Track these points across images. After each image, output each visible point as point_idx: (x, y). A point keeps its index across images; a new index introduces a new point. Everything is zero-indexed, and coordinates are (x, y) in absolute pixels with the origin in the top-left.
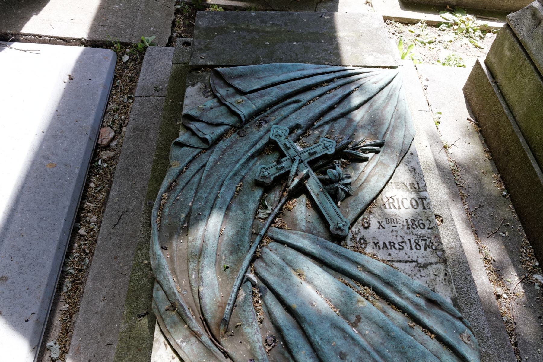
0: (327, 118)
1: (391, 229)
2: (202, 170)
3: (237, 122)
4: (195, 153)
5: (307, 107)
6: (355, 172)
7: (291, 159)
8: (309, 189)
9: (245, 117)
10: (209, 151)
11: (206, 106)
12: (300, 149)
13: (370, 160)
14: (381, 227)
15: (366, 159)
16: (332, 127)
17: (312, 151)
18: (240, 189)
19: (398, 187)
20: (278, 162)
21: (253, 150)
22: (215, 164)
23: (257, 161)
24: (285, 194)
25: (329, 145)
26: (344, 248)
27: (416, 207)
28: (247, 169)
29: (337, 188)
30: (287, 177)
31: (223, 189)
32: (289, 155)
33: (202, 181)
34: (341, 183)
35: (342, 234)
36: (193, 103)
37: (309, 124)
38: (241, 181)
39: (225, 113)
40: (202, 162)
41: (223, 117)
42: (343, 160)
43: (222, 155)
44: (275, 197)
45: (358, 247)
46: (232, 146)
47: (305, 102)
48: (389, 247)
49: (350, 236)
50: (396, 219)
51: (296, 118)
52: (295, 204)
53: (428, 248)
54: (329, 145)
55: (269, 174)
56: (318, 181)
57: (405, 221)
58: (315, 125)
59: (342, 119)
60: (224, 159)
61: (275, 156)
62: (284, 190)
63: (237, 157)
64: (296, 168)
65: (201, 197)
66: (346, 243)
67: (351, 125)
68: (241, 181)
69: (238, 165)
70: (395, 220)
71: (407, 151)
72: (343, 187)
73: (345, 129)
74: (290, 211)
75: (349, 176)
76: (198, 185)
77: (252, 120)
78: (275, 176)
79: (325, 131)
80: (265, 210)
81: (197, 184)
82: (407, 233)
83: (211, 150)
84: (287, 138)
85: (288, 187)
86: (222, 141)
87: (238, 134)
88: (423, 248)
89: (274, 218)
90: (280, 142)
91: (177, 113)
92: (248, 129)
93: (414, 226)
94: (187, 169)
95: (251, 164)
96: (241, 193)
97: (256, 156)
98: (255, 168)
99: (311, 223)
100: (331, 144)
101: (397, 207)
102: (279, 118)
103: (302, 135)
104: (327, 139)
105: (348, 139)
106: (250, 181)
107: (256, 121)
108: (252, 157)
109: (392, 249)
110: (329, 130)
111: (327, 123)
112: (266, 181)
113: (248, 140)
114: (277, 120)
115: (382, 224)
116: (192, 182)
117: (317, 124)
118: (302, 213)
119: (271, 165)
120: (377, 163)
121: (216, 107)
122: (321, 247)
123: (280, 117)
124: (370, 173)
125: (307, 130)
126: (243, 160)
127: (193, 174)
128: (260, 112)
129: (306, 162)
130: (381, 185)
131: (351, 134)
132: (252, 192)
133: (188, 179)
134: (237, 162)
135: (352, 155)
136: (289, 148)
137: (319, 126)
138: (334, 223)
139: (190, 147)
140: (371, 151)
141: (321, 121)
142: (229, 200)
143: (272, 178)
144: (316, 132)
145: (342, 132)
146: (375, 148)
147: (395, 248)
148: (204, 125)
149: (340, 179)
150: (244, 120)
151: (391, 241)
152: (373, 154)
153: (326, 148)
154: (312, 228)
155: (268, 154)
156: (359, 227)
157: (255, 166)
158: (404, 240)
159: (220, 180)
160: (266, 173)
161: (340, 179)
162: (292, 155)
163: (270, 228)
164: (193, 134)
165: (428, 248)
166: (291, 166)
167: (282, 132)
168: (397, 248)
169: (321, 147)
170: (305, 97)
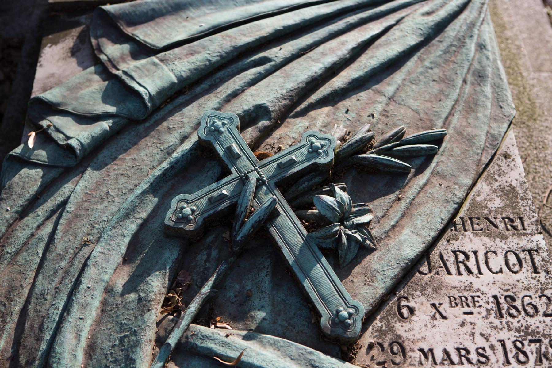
1: (460, 320)
14: (438, 316)
25: (322, 146)
27: (517, 268)
37: (285, 106)
48: (456, 359)
50: (473, 297)
53: (544, 360)
70: (470, 299)
82: (495, 328)
88: (532, 358)
93: (513, 311)
101: (475, 270)
109: (462, 364)
115: (441, 309)
147: (469, 361)
151: (461, 346)
165: (544, 360)
168: (474, 361)
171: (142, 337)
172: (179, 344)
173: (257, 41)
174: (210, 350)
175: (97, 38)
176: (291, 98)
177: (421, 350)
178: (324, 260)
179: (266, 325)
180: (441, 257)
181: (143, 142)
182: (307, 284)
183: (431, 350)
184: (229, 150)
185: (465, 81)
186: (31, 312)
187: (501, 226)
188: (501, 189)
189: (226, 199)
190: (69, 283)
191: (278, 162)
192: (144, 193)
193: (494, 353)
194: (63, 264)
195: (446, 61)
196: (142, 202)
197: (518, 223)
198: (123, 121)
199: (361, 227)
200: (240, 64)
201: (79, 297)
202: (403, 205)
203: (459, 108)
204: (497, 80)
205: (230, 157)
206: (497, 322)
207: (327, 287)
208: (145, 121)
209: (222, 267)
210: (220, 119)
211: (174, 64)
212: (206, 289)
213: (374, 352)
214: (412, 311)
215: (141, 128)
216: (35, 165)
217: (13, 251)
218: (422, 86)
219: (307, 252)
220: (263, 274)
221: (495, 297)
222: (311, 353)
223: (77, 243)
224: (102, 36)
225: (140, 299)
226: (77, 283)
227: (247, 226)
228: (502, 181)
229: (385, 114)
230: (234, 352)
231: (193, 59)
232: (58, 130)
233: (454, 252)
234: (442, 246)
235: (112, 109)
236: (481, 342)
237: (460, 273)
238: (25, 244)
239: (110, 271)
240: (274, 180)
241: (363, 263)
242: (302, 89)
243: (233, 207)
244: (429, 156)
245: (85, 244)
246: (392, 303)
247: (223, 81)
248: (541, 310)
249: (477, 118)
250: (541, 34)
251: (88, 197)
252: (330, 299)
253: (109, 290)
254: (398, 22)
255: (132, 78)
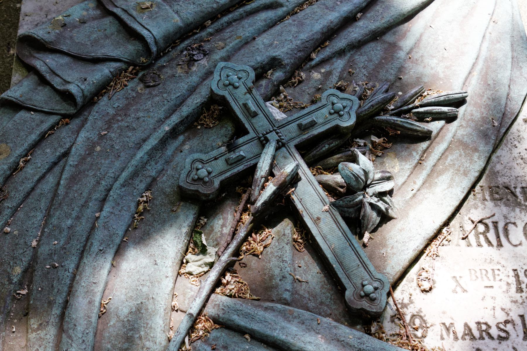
0: (340, 43)
2: (61, 163)
3: (139, 54)
4: (45, 126)
5: (294, 17)
6: (400, 165)
7: (259, 138)
8: (299, 206)
9: (156, 42)
10: (77, 122)
11: (71, 18)
12: (278, 115)
13: (436, 137)
14: (459, 289)
15: (426, 136)
16: (351, 64)
17: (305, 121)
18: (145, 209)
19: (497, 196)
20: (231, 147)
21: (175, 119)
22: (90, 150)
23: (183, 143)
24: (247, 218)
25: (344, 107)
26: (376, 341)
28: (161, 162)
29: (361, 202)
30: (250, 179)
31: (107, 208)
32: (255, 130)
33: (61, 191)
34: (370, 191)
35: (374, 309)
36: (41, 9)
37: (300, 58)
38: (147, 189)
39: (112, 34)
40: (61, 146)
41: (107, 41)
42: (374, 139)
43: (106, 130)
44: (223, 226)
45: (407, 336)
46: (128, 109)
47: (290, 7)
49: (390, 312)
51: (271, 45)
52: (269, 241)
54: (344, 107)
55: (209, 173)
56: (320, 189)
57: (512, 273)
58: (312, 59)
59: (372, 45)
60: (111, 139)
61: (223, 131)
62: (245, 210)
63: (139, 135)
64: (269, 161)
65: (58, 227)
66: (381, 328)
67: (392, 57)
68: (147, 189)
69: (140, 154)
70: (490, 272)
71: (517, 115)
72: (374, 200)
73: (379, 66)
74: (257, 256)
75: (388, 175)
76: (53, 199)
77: (172, 48)
78: (223, 177)
79: (334, 72)
80: (201, 256)
81: (50, 196)
83: (82, 118)
84: (250, 91)
85: (253, 203)
86: (105, 98)
87: (142, 80)
89: (223, 274)
90: (235, 100)
91: (9, 28)
92: (165, 70)
94: (26, 162)
95: (169, 151)
96: (147, 217)
97: (183, 133)
98: (178, 158)
99: (304, 285)
100: (349, 103)
101: (494, 242)
102: (232, 44)
103: (284, 82)
104: (338, 93)
105: (387, 91)
106: (168, 190)
107: (182, 52)
108: (174, 133)
110: (343, 70)
111: (341, 53)
112: (203, 190)
113: (165, 95)
114: (228, 48)
115: (461, 282)
116: (38, 191)
117: (317, 58)
118: (283, 261)
119: (215, 153)
120: (451, 143)
121: (94, 19)
122: (326, 340)
123: (237, 41)
124: (434, 166)
125: (294, 72)
126: (153, 142)
127: (40, 174)
128: (191, 31)
129: (292, 144)
130: (459, 193)
131: (392, 78)
132: (173, 214)
133: (29, 185)
134: (139, 146)
135: (395, 126)
136: (255, 115)
137: (323, 62)
138: (354, 285)
139: (35, 111)
140: (437, 117)
141: (327, 49)
142: (121, 233)
143: (217, 183)
144: (316, 75)
145: (372, 76)
146: (445, 109)
147: (491, 337)
148: (65, 60)
149: (369, 182)
150: (154, 49)
151: (482, 321)
152: (442, 122)
153: (337, 112)
154: (307, 295)
155: (208, 128)
156: (412, 292)
157: (180, 155)
158: (509, 318)
159: (101, 188)
160: (203, 173)
161: (369, 182)
162: (261, 131)
163: (213, 296)
164: (43, 81)
166: (258, 156)
167: (240, 78)
168: (495, 337)
169: (325, 111)
171: (161, 306)
189: (244, 160)
191: (297, 122)
193: (514, 328)
205: (244, 113)
211: (178, 4)
217: (14, 206)
222: (335, 327)
230: (258, 324)
237: (479, 245)
240: (294, 142)
252: (355, 272)
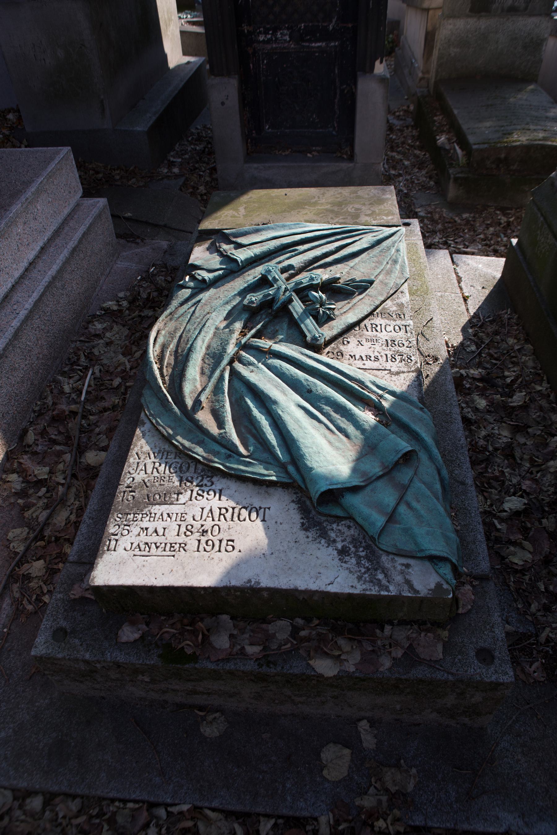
27: (398, 331)
37: (302, 266)
88: (398, 361)
101: (379, 330)
147: (370, 360)
170: (301, 248)
172: (245, 343)
173: (292, 242)
174: (258, 346)
175: (219, 243)
176: (305, 263)
177: (350, 355)
178: (311, 317)
179: (283, 340)
180: (365, 325)
181: (236, 280)
182: (302, 326)
183: (354, 356)
184: (274, 278)
185: (387, 263)
186: (184, 335)
187: (394, 317)
188: (397, 304)
190: (200, 326)
192: (235, 295)
194: (198, 320)
195: (380, 255)
196: (234, 298)
197: (402, 316)
198: (228, 271)
199: (329, 309)
200: (284, 252)
201: (205, 329)
202: (350, 305)
203: (382, 273)
204: (403, 264)
206: (385, 348)
207: (311, 327)
208: (238, 272)
209: (267, 320)
210: (271, 267)
212: (259, 326)
213: (330, 354)
214: (348, 342)
215: (236, 274)
216: (188, 288)
218: (367, 264)
219: (304, 314)
220: (284, 323)
221: (386, 340)
223: (205, 313)
224: (221, 242)
225: (230, 330)
226: (205, 324)
227: (279, 303)
228: (398, 301)
229: (348, 273)
231: (262, 248)
232: (199, 275)
233: (371, 324)
234: (366, 322)
235: (224, 267)
236: (376, 354)
238: (182, 314)
239: (218, 322)
241: (329, 323)
242: (311, 260)
243: (273, 298)
244: (365, 289)
245: (208, 313)
246: (340, 339)
247: (275, 258)
248: (406, 345)
249: (391, 277)
250: (448, 276)
251: (210, 298)
253: (217, 328)
254: (360, 239)
255: (234, 255)
